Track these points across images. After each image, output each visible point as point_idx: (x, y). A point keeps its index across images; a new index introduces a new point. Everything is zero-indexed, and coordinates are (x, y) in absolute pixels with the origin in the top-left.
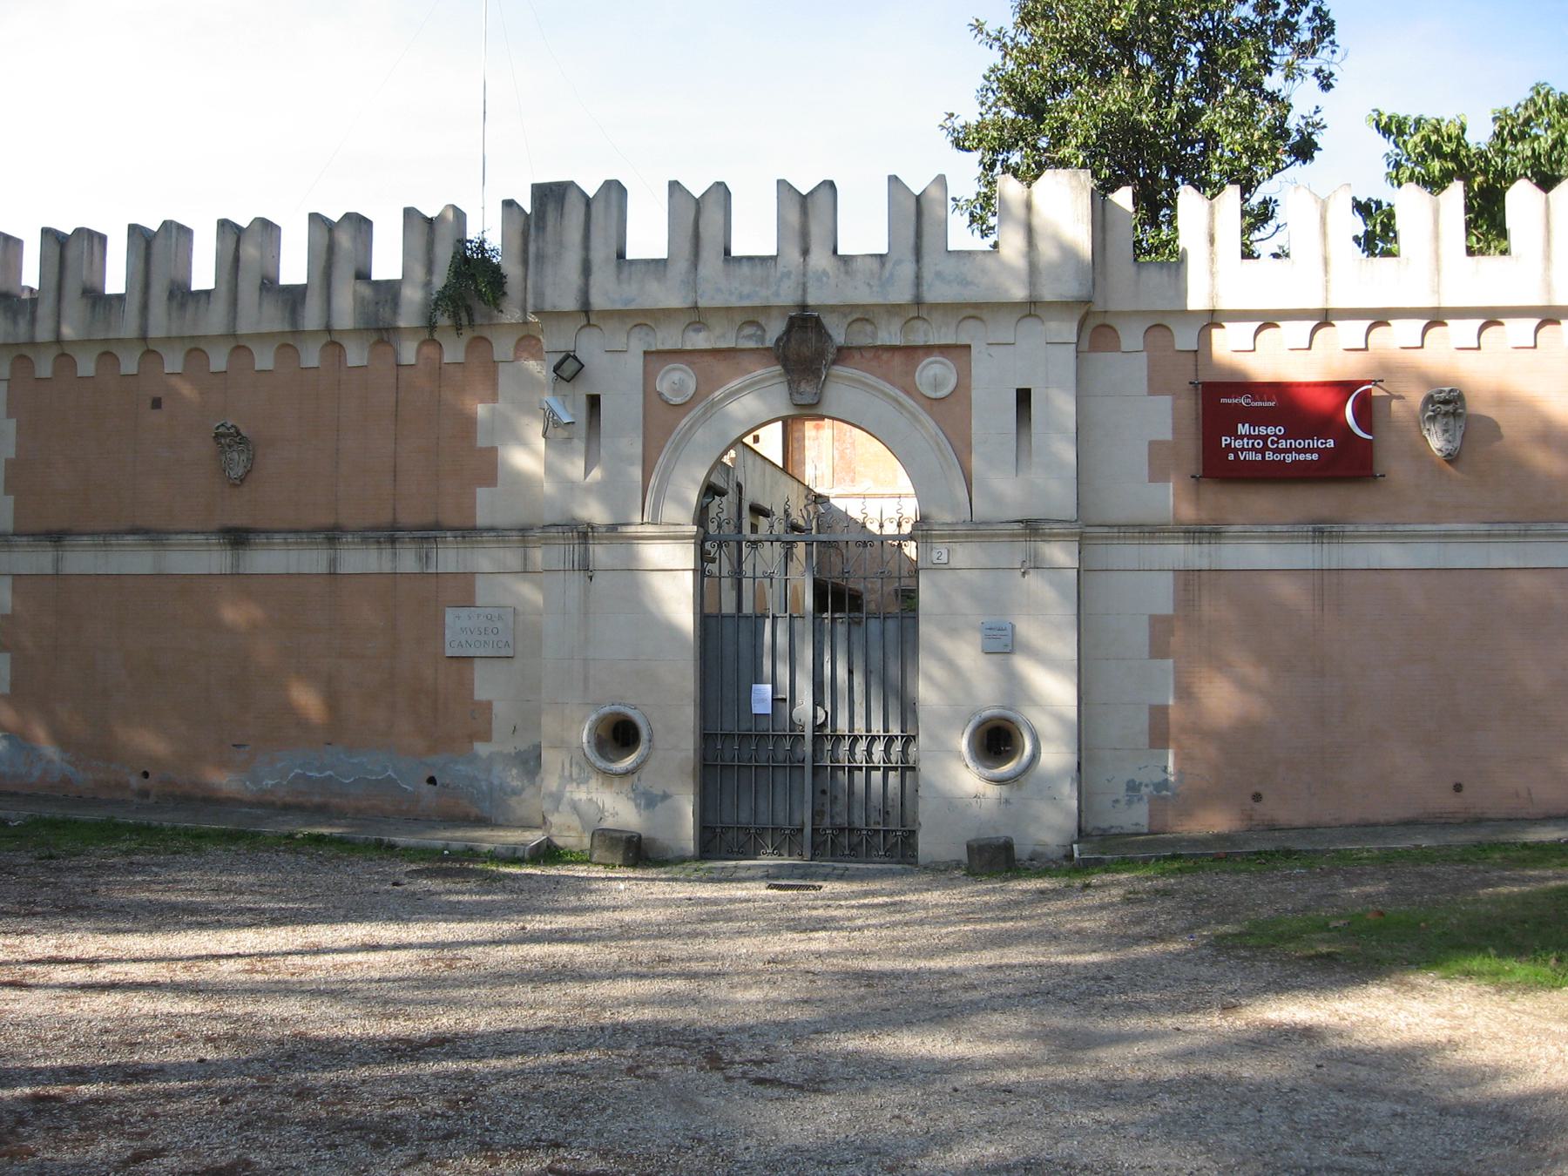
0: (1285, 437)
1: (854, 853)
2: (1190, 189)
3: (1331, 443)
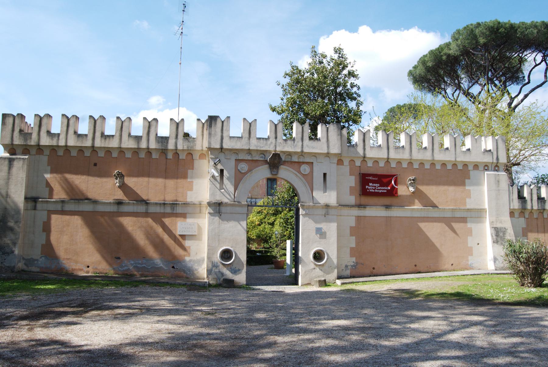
0: (379, 186)
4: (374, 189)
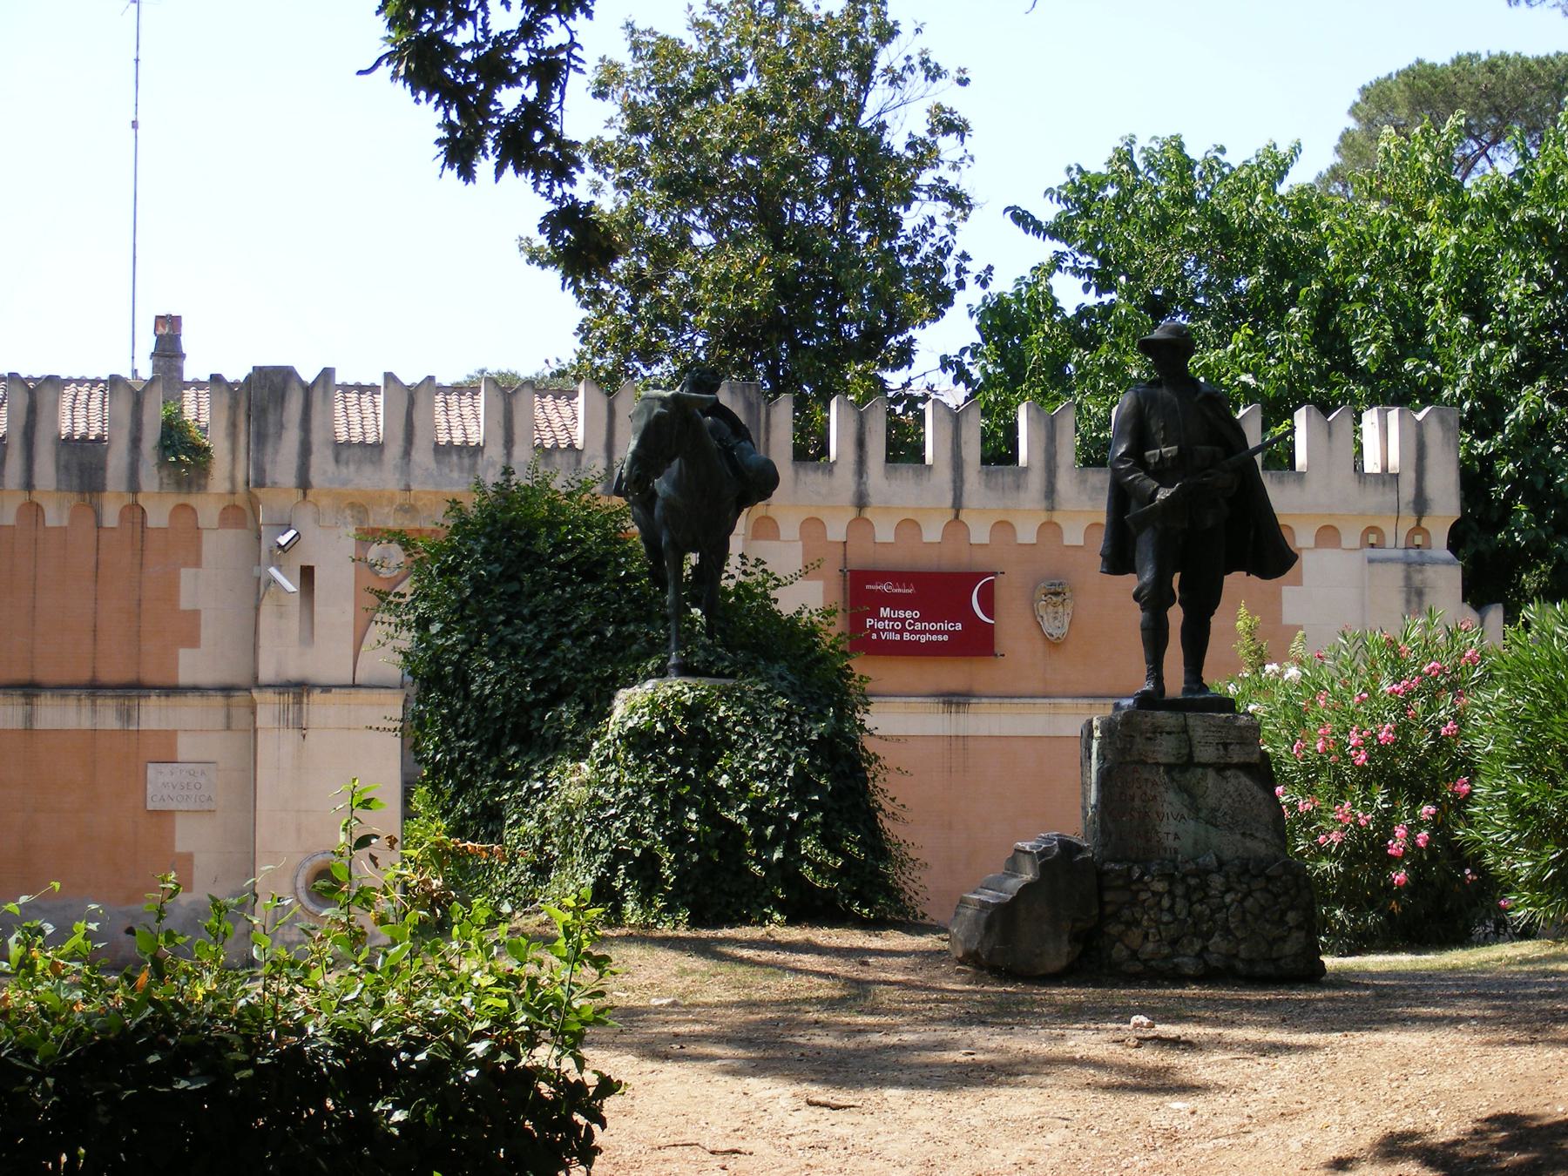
0: (920, 620)
1: (1489, 984)
2: (124, 375)
3: (959, 627)
4: (897, 632)
